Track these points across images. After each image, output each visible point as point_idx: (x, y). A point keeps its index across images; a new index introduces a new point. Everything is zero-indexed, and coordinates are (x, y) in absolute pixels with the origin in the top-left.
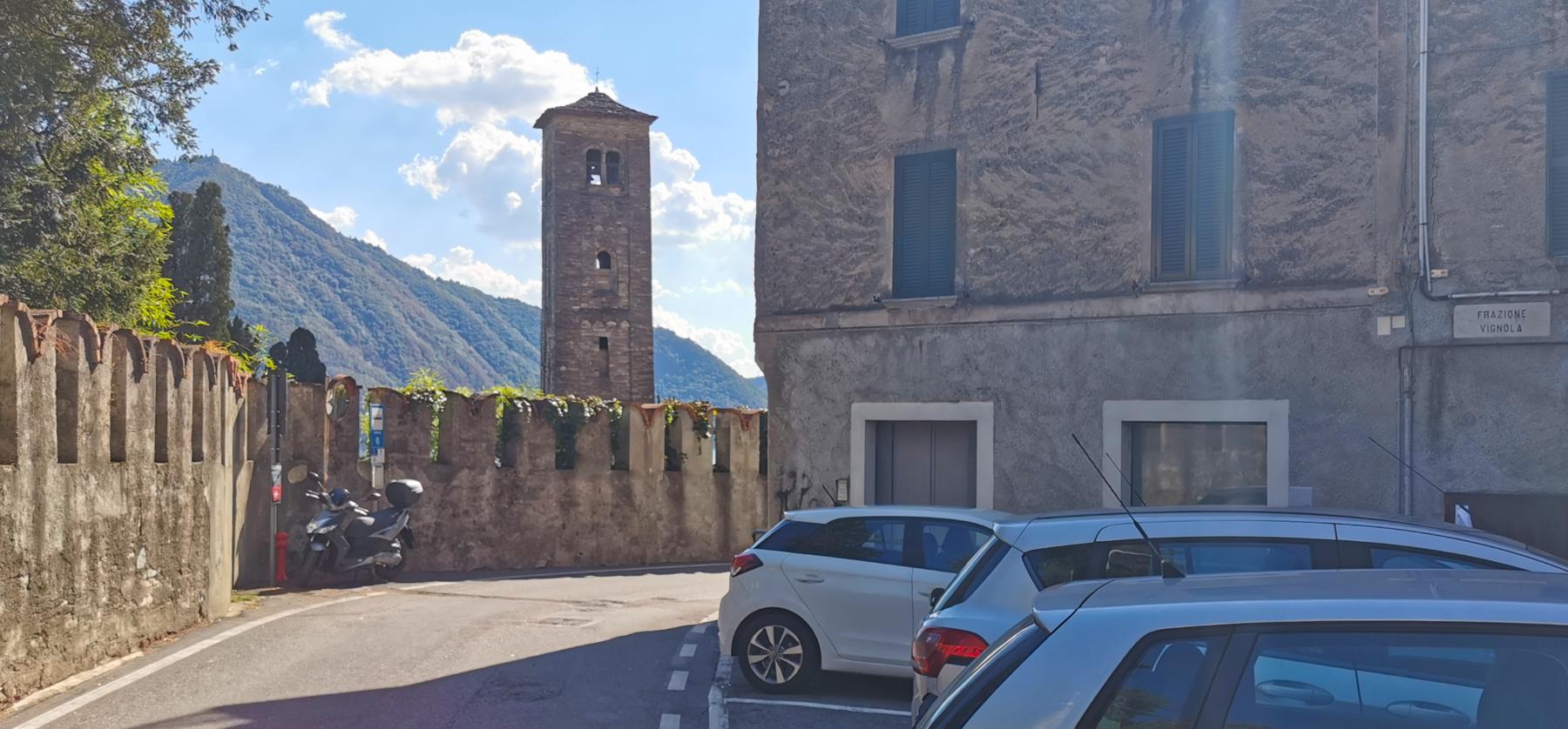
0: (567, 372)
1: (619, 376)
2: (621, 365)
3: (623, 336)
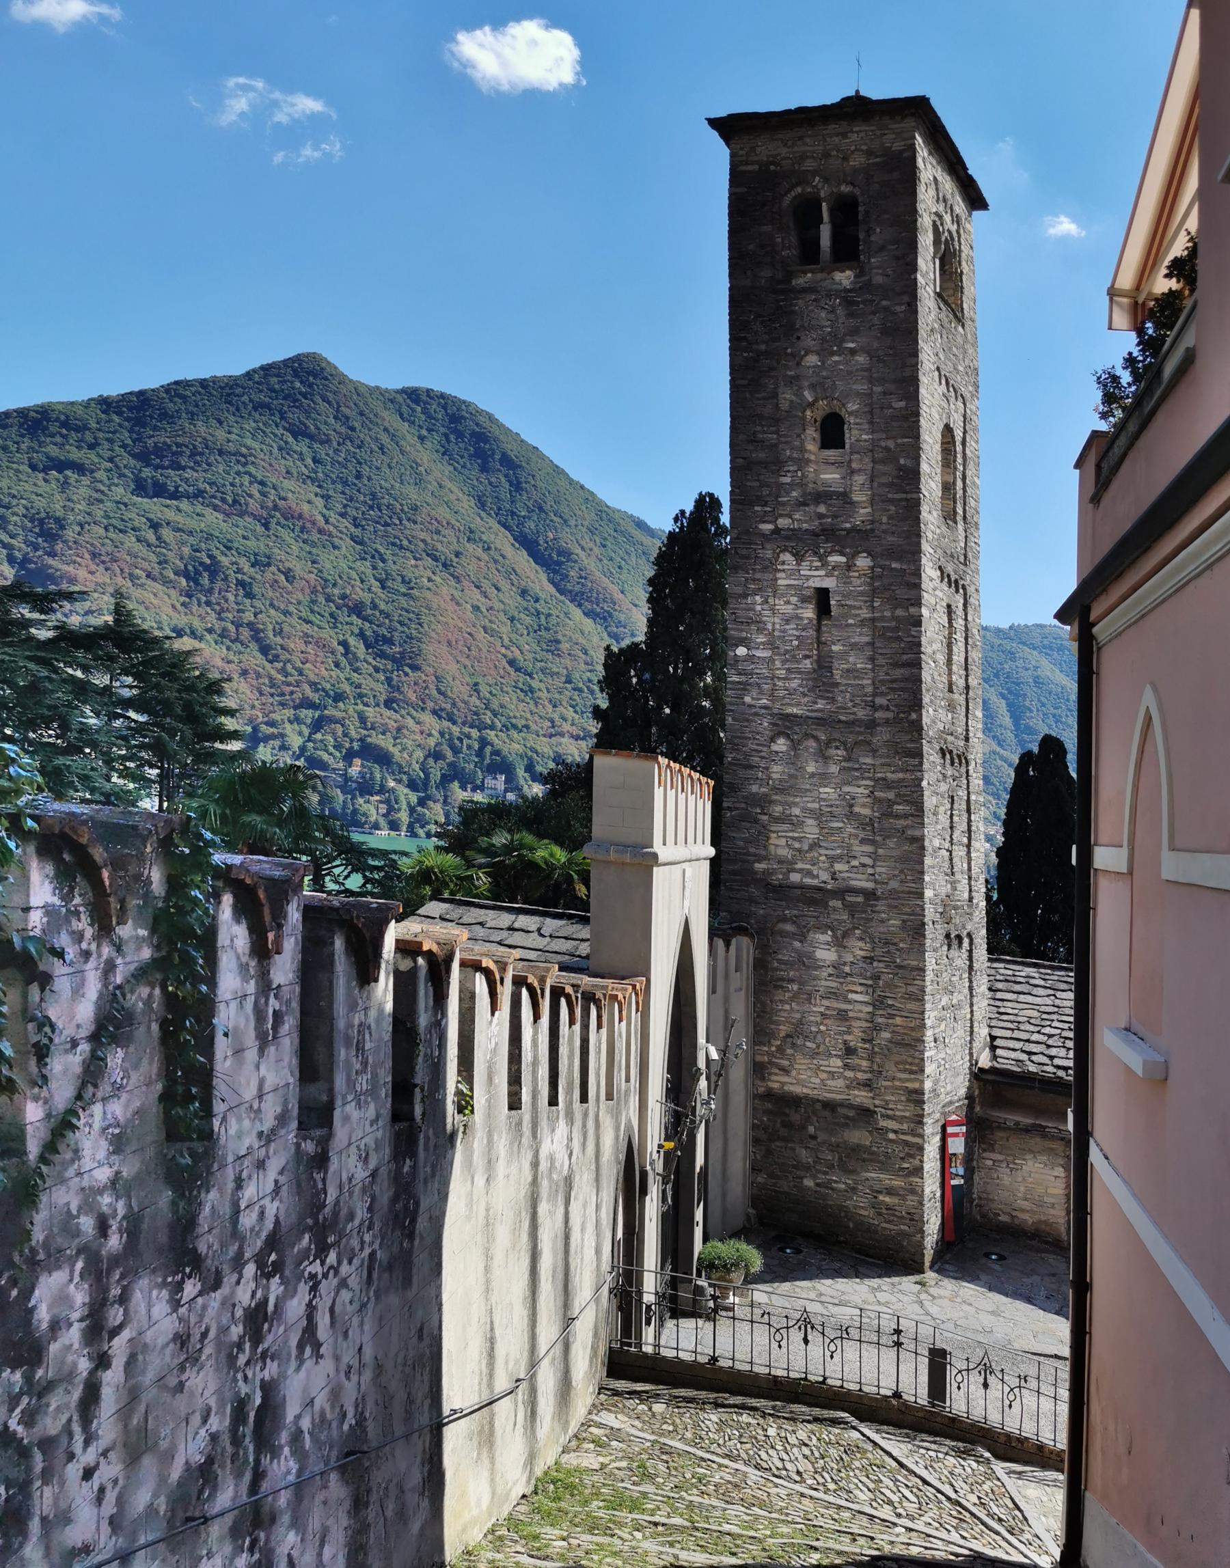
0: (750, 658)
3: (858, 584)
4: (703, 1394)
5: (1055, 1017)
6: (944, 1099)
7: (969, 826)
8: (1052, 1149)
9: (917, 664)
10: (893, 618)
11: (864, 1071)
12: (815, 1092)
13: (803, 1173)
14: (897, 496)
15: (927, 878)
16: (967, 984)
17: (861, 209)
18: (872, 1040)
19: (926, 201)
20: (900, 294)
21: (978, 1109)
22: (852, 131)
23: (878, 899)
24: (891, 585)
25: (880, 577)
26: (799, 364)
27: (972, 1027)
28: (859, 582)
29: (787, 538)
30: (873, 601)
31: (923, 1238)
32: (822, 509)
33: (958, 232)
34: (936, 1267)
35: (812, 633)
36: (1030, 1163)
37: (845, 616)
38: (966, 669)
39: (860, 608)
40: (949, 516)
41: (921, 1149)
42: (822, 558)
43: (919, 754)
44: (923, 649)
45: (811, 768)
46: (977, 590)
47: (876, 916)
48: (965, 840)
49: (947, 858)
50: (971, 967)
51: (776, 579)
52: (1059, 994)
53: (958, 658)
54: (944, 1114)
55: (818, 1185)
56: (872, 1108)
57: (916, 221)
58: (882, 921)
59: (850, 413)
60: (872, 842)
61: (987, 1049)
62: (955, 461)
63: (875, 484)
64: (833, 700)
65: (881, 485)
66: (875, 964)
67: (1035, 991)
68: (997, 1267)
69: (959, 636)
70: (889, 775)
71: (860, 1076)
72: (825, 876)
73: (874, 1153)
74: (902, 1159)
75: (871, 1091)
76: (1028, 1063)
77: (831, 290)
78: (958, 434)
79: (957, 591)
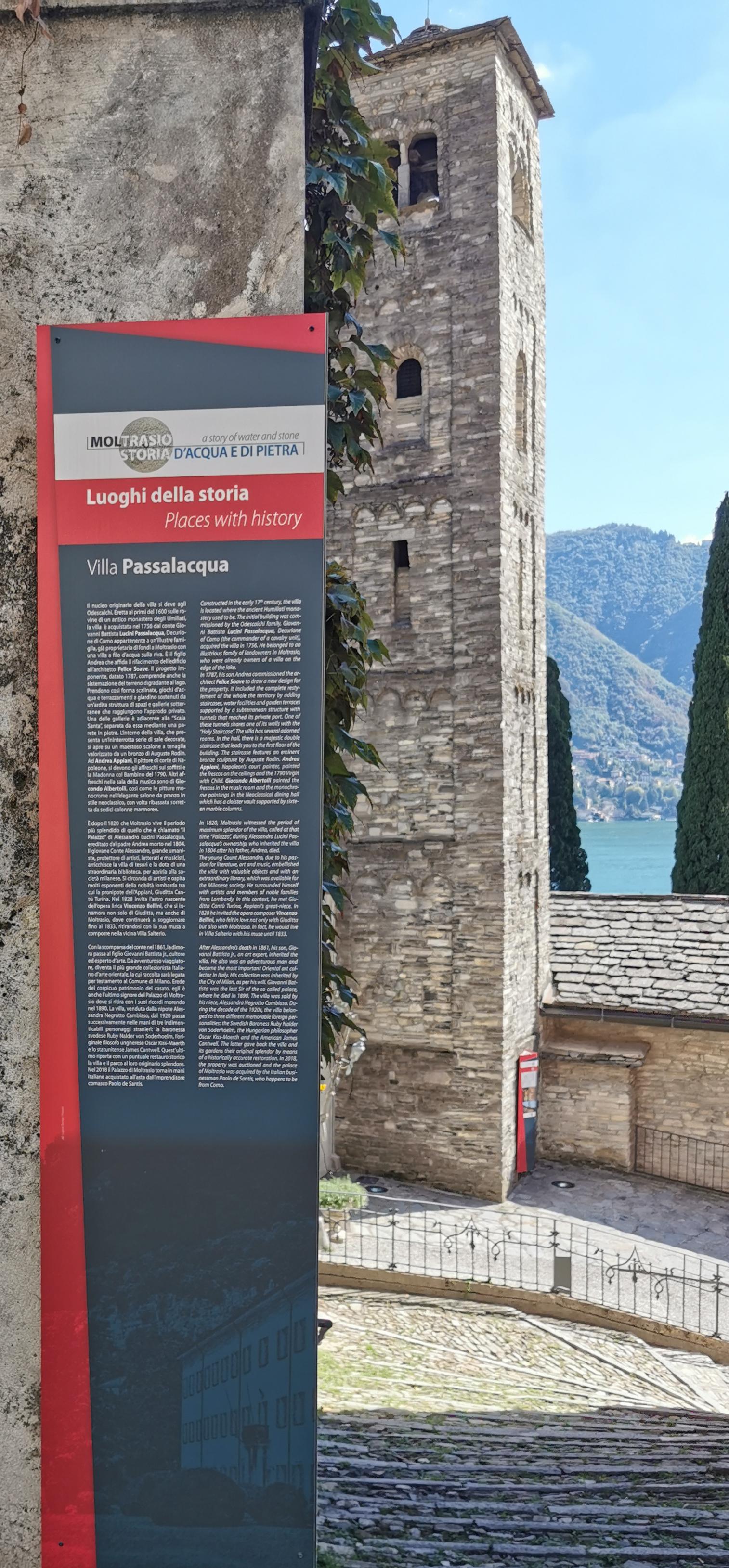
1: (431, 621)
2: (433, 596)
3: (437, 532)
4: (387, 1296)
5: (612, 947)
6: (517, 1035)
7: (536, 762)
8: (617, 1077)
9: (496, 606)
10: (471, 561)
11: (444, 1015)
12: (396, 1038)
13: (384, 1117)
14: (476, 436)
15: (505, 819)
16: (533, 921)
17: (440, 144)
18: (452, 982)
19: (504, 124)
20: (479, 226)
21: (541, 1044)
22: (431, 66)
23: (457, 845)
24: (469, 528)
25: (459, 521)
26: (377, 314)
27: (537, 963)
28: (437, 529)
29: (365, 495)
30: (451, 547)
31: (501, 1169)
32: (400, 461)
33: (528, 148)
34: (511, 1197)
35: (390, 587)
36: (594, 1093)
37: (423, 566)
38: (533, 602)
39: (439, 556)
40: (521, 447)
41: (499, 1084)
42: (400, 511)
43: (498, 696)
44: (501, 590)
45: (390, 723)
46: (542, 519)
47: (455, 861)
48: (532, 777)
49: (518, 797)
50: (537, 904)
51: (354, 538)
52: (612, 924)
53: (527, 593)
54: (517, 1050)
55: (398, 1127)
56: (451, 1049)
57: (496, 147)
58: (462, 866)
59: (429, 358)
60: (451, 789)
61: (550, 985)
62: (525, 388)
63: (454, 427)
64: (412, 651)
65: (459, 427)
66: (455, 909)
67: (589, 923)
68: (568, 1194)
69: (528, 571)
70: (469, 721)
71: (440, 1019)
72: (404, 828)
73: (453, 1092)
74: (481, 1095)
75: (450, 1032)
76: (591, 994)
77: (409, 233)
78: (529, 358)
79: (527, 524)
